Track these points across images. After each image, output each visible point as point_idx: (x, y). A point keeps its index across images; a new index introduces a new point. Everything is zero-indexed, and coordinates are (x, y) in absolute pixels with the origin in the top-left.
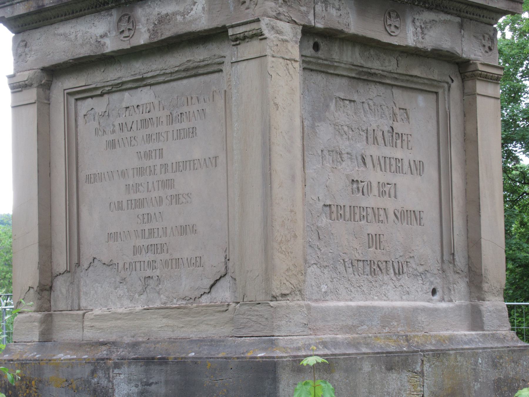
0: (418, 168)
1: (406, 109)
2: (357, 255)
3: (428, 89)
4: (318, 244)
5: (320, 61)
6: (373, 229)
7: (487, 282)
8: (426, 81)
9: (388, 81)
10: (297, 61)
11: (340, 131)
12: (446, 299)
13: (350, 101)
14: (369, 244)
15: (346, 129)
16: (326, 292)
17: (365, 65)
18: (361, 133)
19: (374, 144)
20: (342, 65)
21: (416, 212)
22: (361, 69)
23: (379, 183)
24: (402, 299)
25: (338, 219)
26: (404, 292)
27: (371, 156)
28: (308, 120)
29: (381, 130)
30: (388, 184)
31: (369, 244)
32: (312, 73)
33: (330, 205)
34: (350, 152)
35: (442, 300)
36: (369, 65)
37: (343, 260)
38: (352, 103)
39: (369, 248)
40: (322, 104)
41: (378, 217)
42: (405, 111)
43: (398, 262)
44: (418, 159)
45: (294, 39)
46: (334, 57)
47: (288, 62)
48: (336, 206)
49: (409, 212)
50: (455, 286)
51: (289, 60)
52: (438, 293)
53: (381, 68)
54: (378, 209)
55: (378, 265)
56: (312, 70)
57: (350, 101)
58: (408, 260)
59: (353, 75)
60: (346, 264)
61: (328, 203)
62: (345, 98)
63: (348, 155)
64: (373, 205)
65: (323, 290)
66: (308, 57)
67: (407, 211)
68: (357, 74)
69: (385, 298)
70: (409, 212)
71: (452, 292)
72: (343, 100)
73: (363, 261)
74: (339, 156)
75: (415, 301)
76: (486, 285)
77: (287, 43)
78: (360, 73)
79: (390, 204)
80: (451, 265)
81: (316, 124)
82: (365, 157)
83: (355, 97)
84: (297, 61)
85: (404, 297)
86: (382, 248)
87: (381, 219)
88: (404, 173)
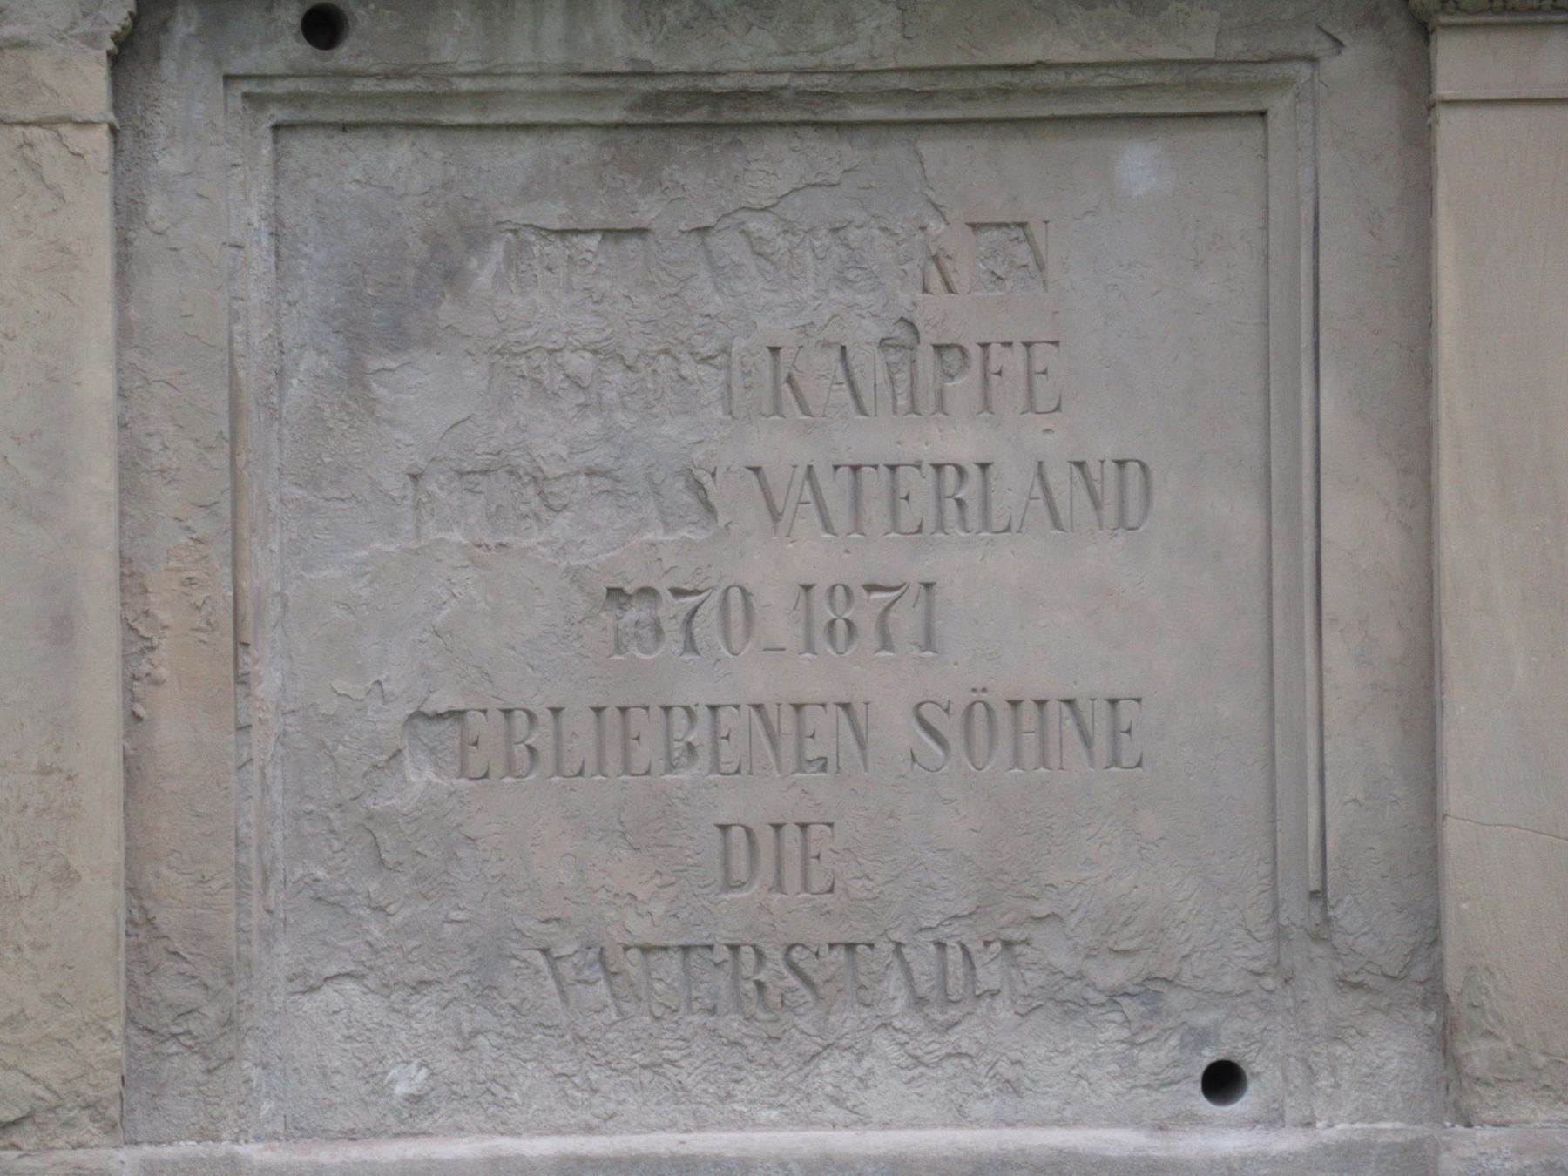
0: (1118, 492)
1: (1022, 225)
2: (632, 923)
3: (1180, 109)
4: (373, 886)
5: (358, 86)
6: (757, 801)
7: (1489, 1034)
8: (1143, 76)
9: (858, 113)
10: (88, 124)
11: (545, 376)
12: (1290, 1115)
13: (612, 234)
14: (726, 865)
15: (580, 363)
16: (415, 1099)
17: (659, 61)
18: (685, 371)
19: (777, 410)
20: (513, 83)
21: (771, 710)
22: (643, 86)
23: (807, 588)
24: (961, 1118)
25: (510, 769)
26: (979, 1085)
27: (756, 470)
28: (320, 352)
29: (826, 345)
30: (871, 588)
31: (726, 865)
32: (348, 138)
33: (457, 715)
34: (609, 464)
35: (1273, 1119)
36: (698, 56)
37: (545, 951)
38: (633, 243)
39: (729, 885)
40: (411, 272)
41: (626, 750)
42: (1019, 232)
43: (941, 945)
44: (1103, 449)
45: (85, 27)
46: (446, 54)
47: (35, 133)
48: (657, 713)
49: (1028, 709)
50: (1340, 1049)
51: (38, 124)
52: (1252, 1086)
53: (778, 61)
54: (798, 707)
55: (794, 968)
56: (344, 127)
57: (612, 234)
58: (1014, 934)
59: (616, 115)
60: (566, 968)
61: (443, 701)
62: (572, 225)
63: (596, 481)
64: (759, 689)
65: (401, 1089)
66: (273, 77)
67: (1015, 704)
68: (632, 108)
69: (832, 1112)
70: (1028, 709)
71: (1324, 1082)
72: (562, 233)
73: (686, 949)
74: (530, 491)
75: (1061, 1123)
76: (1484, 1045)
77: (22, 53)
78: (655, 101)
79: (888, 685)
80: (1318, 950)
81: (374, 364)
82: (706, 480)
83: (649, 211)
84: (88, 124)
85: (978, 1108)
86: (818, 882)
87: (810, 754)
88: (999, 524)
